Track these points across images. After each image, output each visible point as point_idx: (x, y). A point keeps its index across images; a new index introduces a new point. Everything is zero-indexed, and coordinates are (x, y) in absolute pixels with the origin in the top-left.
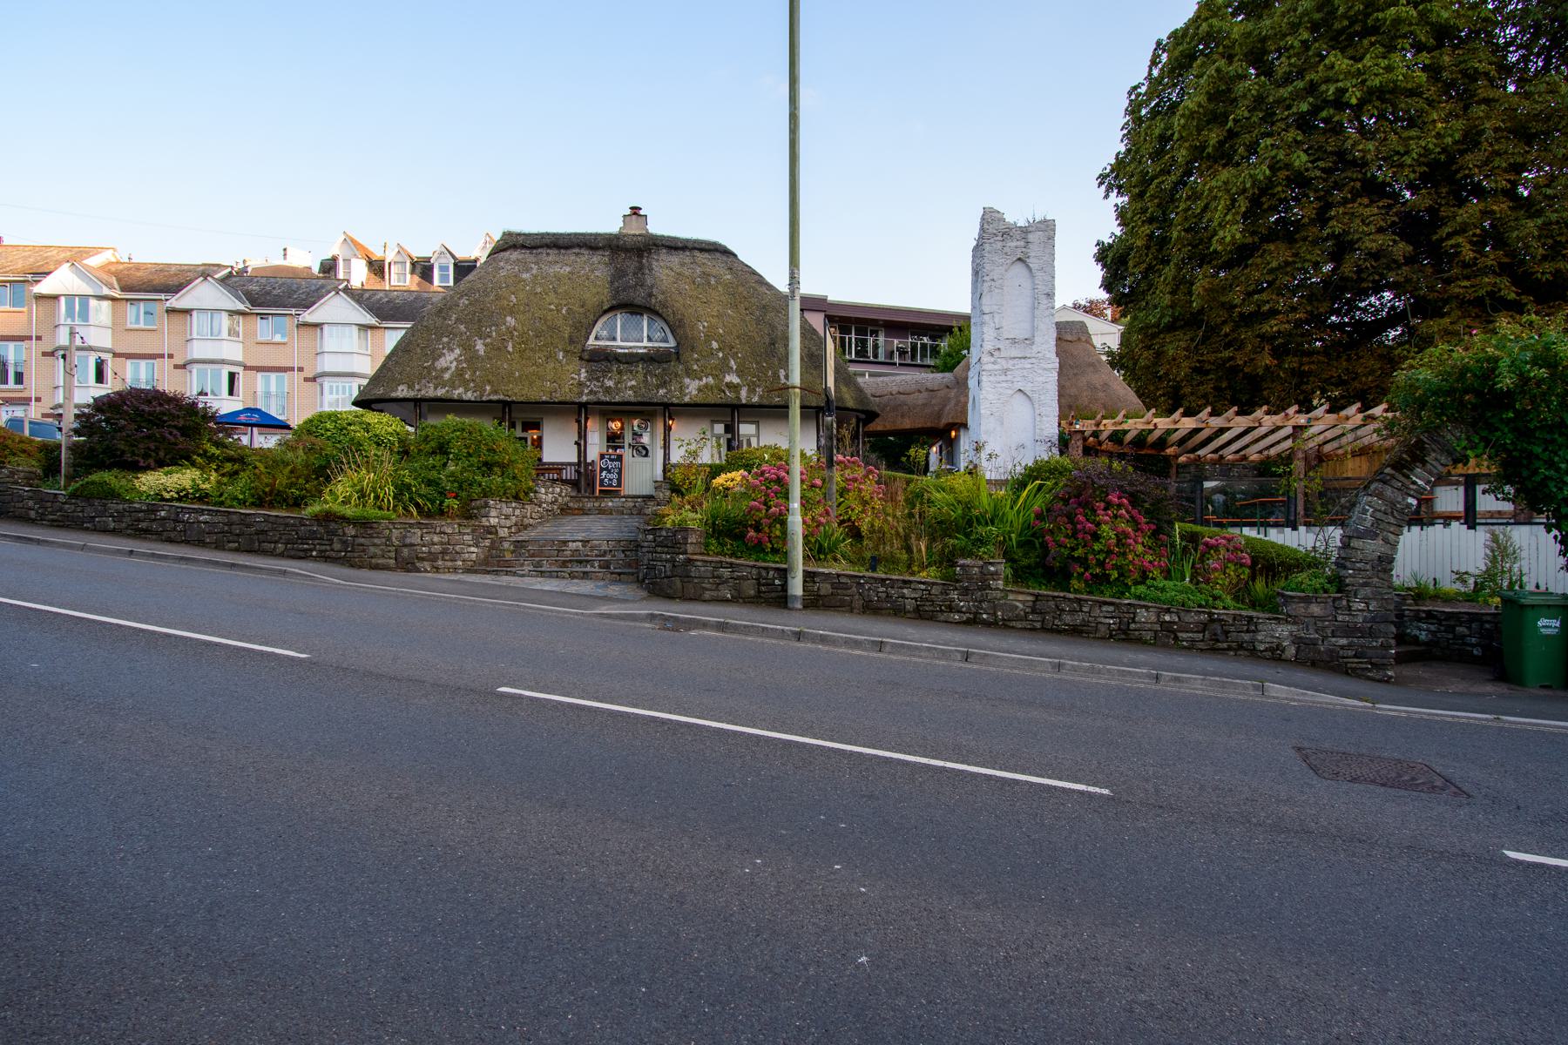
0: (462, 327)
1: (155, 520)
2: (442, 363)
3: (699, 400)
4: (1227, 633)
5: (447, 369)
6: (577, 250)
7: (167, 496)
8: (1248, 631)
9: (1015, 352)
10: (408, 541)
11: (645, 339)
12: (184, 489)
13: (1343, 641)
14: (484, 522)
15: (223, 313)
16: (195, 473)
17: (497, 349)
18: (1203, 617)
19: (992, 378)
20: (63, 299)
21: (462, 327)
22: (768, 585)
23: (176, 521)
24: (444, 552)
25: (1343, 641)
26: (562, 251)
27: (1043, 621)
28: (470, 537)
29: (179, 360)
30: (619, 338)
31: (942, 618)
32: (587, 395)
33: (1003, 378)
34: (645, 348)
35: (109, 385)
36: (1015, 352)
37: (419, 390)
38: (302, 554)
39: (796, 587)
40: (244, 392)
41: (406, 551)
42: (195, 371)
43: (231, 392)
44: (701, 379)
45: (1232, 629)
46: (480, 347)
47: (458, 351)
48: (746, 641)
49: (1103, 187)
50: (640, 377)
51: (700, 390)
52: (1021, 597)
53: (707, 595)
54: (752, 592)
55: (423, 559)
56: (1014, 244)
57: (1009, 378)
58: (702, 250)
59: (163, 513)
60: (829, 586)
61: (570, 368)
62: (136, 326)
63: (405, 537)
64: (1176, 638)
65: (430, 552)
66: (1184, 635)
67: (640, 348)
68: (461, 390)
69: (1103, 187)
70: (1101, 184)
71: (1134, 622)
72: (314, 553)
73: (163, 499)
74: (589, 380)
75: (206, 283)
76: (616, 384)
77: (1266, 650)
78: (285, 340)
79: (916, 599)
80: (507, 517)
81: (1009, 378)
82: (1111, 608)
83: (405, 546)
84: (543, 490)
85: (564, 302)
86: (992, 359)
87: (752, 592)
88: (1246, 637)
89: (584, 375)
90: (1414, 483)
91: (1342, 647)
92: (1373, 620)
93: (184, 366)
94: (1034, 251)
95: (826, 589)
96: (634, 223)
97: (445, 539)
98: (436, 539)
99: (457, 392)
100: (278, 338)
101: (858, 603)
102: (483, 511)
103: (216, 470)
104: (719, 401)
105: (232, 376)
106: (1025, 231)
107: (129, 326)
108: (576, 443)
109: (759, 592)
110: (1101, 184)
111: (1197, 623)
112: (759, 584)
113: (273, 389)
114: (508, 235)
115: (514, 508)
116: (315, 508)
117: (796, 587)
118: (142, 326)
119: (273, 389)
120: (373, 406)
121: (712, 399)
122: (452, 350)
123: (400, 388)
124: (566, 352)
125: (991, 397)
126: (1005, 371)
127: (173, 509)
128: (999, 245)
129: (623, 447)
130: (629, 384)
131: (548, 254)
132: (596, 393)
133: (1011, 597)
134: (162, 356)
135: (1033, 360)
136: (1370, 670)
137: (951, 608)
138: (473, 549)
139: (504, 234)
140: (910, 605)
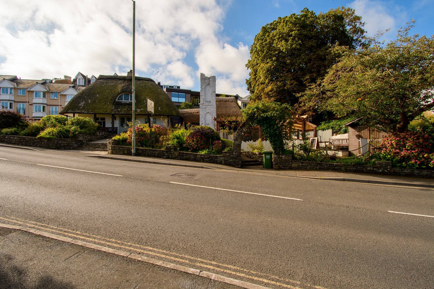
0: (86, 97)
1: (5, 139)
2: (80, 105)
3: (140, 113)
4: (212, 159)
5: (81, 106)
6: (115, 80)
7: (8, 133)
8: (216, 159)
9: (207, 104)
10: (59, 143)
11: (130, 100)
12: (12, 132)
13: (232, 160)
14: (79, 139)
15: (42, 92)
16: (16, 129)
17: (94, 102)
18: (209, 156)
19: (202, 110)
20: (1, 88)
21: (86, 97)
22: (129, 151)
23: (10, 139)
24: (68, 145)
25: (232, 160)
26: (113, 80)
27: (181, 158)
28: (74, 142)
29: (30, 103)
30: (123, 99)
31: (162, 157)
32: (114, 112)
33: (205, 110)
34: (129, 102)
35: (13, 109)
36: (207, 104)
37: (74, 111)
38: (36, 146)
39: (133, 151)
40: (47, 111)
41: (58, 145)
42: (34, 106)
43: (43, 111)
44: (141, 109)
45: (213, 158)
46: (90, 101)
47: (84, 102)
48: (300, 199)
49: (247, 67)
50: (127, 108)
51: (140, 111)
52: (177, 153)
53: (118, 153)
54: (126, 153)
55: (62, 147)
56: (207, 81)
57: (206, 109)
58: (146, 80)
59: (7, 137)
60: (141, 151)
61: (110, 106)
62: (20, 95)
63: (58, 142)
64: (204, 160)
65: (64, 145)
66: (205, 160)
67: (128, 102)
68: (84, 111)
69: (247, 67)
70: (246, 67)
71: (197, 157)
72: (38, 146)
73: (8, 134)
74: (114, 109)
75: (38, 85)
76: (121, 110)
77: (219, 162)
78: (57, 99)
79: (157, 153)
80: (86, 138)
81: (206, 109)
82: (193, 155)
83: (58, 144)
84: (98, 133)
85: (111, 91)
86: (202, 105)
87: (126, 153)
88: (216, 160)
89: (113, 108)
90: (243, 130)
91: (232, 161)
92: (236, 156)
93: (32, 105)
94: (211, 82)
95: (140, 152)
96: (130, 74)
97: (68, 143)
98: (65, 142)
99: (83, 111)
100: (55, 98)
101: (147, 154)
102: (79, 137)
103: (21, 128)
104: (144, 114)
105: (44, 107)
106: (209, 78)
107: (18, 95)
108: (111, 123)
109: (128, 152)
110: (246, 67)
111: (207, 157)
112: (128, 151)
113: (54, 110)
114: (100, 76)
115: (88, 137)
116: (39, 136)
117: (133, 151)
118: (21, 95)
119: (54, 110)
120: (64, 114)
121: (142, 113)
122: (83, 102)
123: (70, 110)
124: (110, 103)
125: (202, 114)
126: (205, 108)
127: (9, 136)
128: (204, 81)
129: (124, 124)
130: (124, 110)
131: (109, 80)
132: (115, 112)
133: (175, 153)
134: (26, 102)
135: (211, 106)
136: (236, 166)
137: (164, 155)
138: (75, 145)
139: (100, 76)
140: (156, 155)
